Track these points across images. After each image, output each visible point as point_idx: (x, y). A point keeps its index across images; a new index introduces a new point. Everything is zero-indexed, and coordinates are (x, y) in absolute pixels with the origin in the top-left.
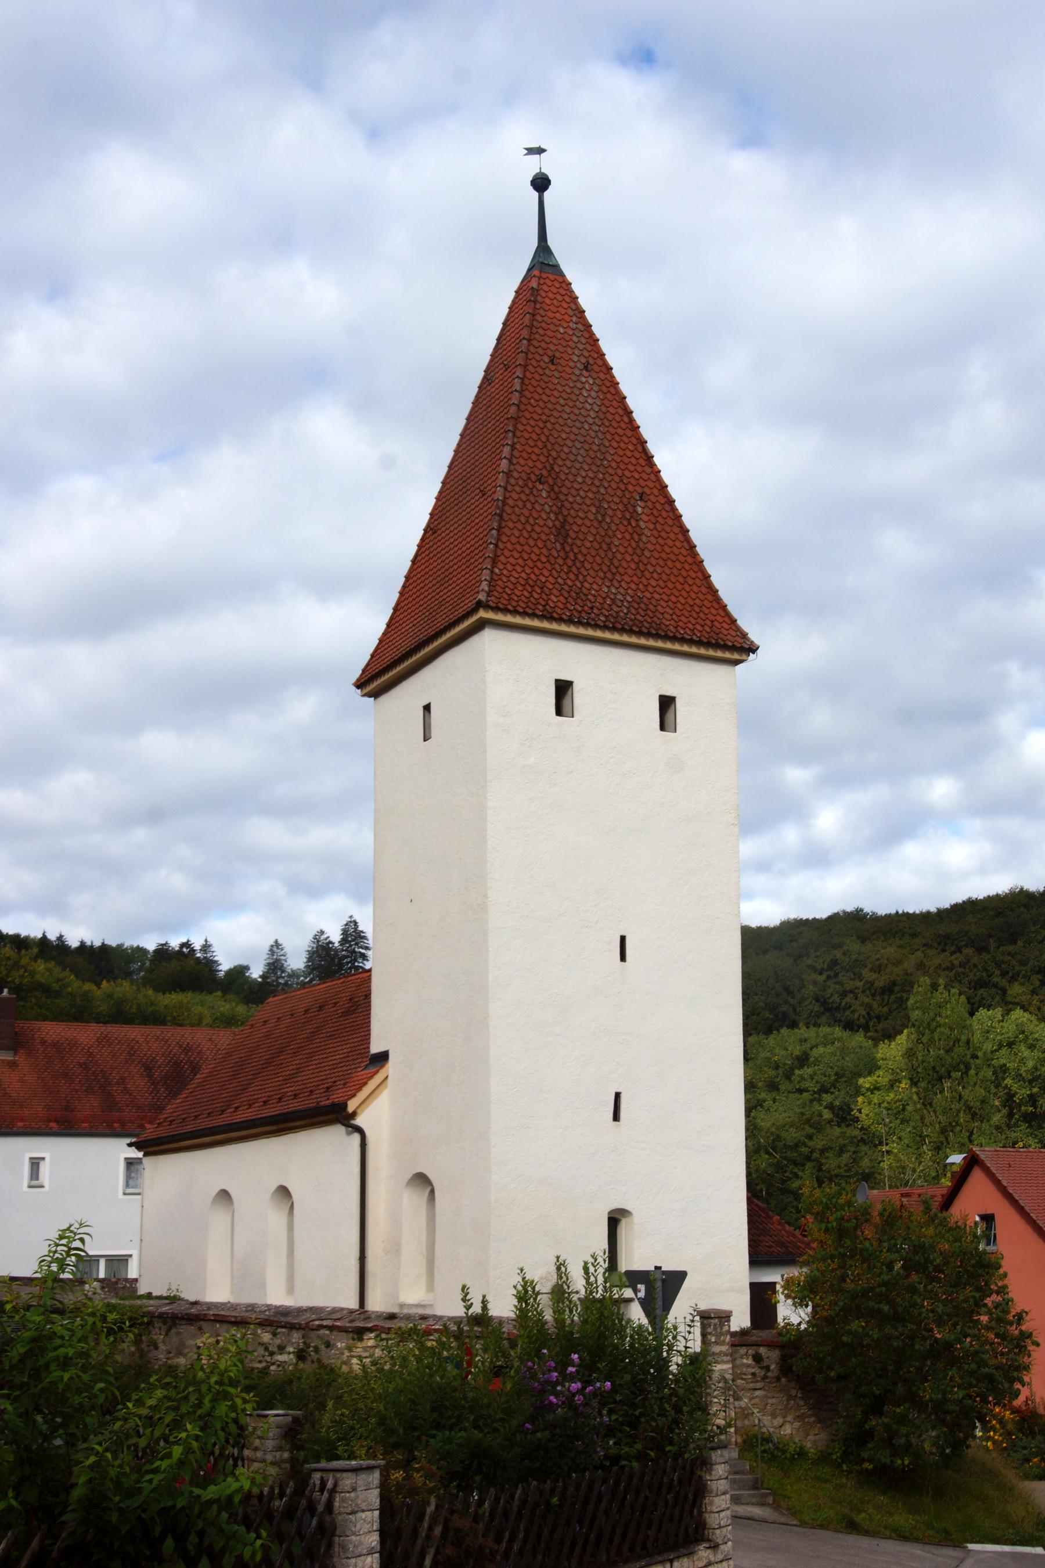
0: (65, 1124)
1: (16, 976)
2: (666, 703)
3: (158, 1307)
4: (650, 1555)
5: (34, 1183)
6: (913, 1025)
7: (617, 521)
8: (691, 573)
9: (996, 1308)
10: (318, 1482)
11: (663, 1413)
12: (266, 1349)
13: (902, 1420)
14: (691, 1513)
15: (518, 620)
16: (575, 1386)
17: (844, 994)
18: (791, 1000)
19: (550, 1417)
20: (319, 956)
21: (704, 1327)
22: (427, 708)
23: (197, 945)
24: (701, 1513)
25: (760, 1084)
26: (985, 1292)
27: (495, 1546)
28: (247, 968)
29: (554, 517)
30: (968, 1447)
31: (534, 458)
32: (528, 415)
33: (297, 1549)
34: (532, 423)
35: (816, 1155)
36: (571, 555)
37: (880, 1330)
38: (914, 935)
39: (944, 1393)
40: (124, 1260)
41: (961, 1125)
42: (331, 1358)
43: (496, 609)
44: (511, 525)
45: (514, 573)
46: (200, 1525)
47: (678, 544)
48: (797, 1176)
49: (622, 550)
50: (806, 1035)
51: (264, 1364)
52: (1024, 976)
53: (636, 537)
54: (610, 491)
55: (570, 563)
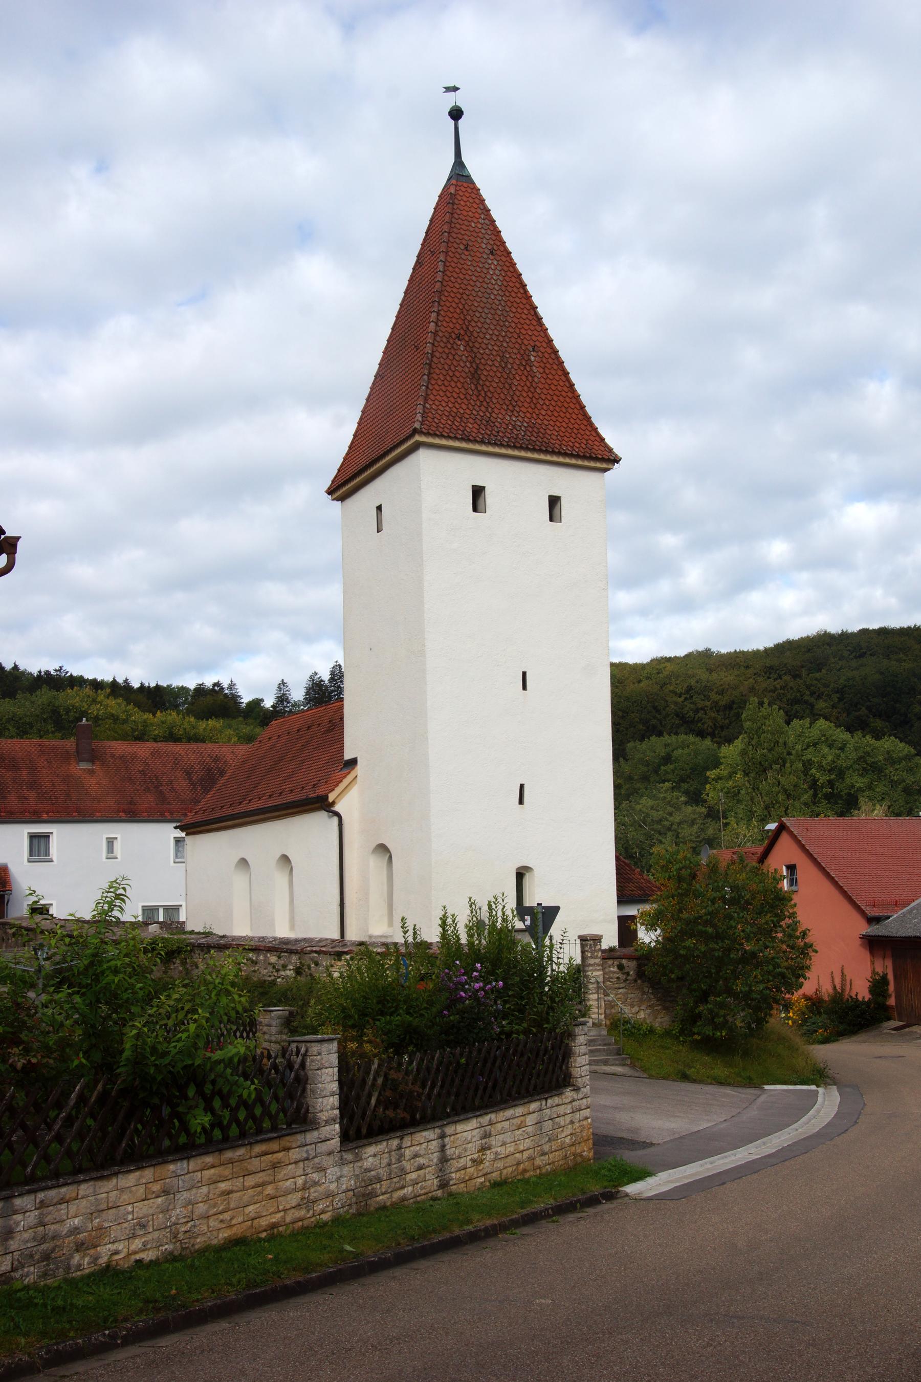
0: (131, 814)
1: (94, 710)
2: (554, 502)
3: (197, 939)
4: (531, 1096)
5: (110, 855)
6: (746, 732)
7: (516, 367)
8: (571, 405)
9: (788, 927)
10: (294, 1050)
11: (541, 1002)
12: (274, 967)
13: (722, 1005)
14: (561, 1068)
15: (443, 442)
16: (477, 985)
17: (697, 711)
18: (658, 716)
19: (460, 1006)
20: (314, 691)
21: (583, 946)
22: (379, 508)
23: (225, 685)
24: (567, 1068)
25: (636, 777)
26: (781, 917)
27: (421, 1090)
28: (262, 700)
29: (471, 363)
30: (767, 1022)
31: (454, 321)
32: (449, 289)
33: (281, 1093)
34: (452, 295)
35: (675, 827)
36: (483, 393)
37: (706, 945)
38: (747, 667)
39: (750, 986)
40: (176, 909)
41: (779, 803)
42: (319, 973)
43: (428, 434)
44: (437, 371)
45: (440, 407)
46: (213, 1077)
47: (561, 383)
48: (661, 842)
49: (520, 389)
50: (669, 741)
51: (273, 978)
52: (827, 695)
53: (530, 378)
54: (510, 344)
55: (481, 399)
